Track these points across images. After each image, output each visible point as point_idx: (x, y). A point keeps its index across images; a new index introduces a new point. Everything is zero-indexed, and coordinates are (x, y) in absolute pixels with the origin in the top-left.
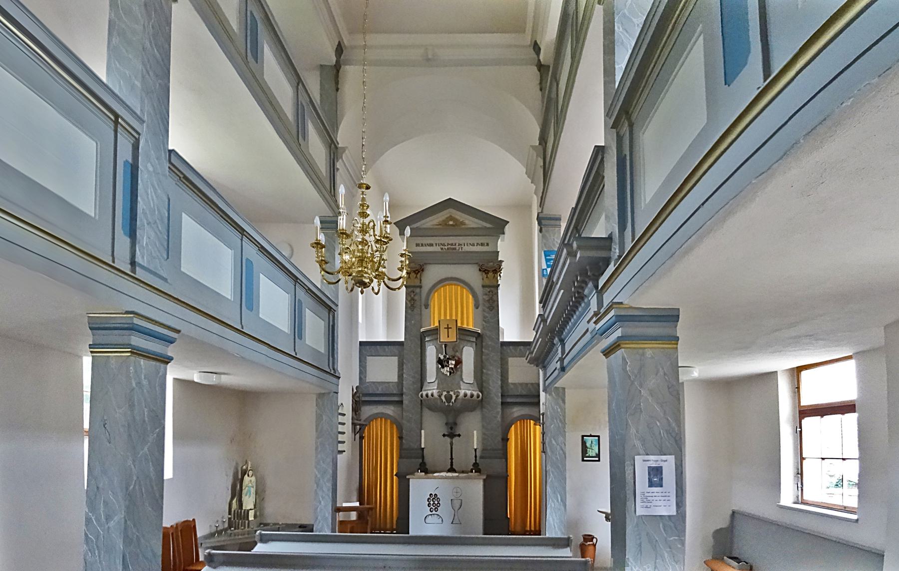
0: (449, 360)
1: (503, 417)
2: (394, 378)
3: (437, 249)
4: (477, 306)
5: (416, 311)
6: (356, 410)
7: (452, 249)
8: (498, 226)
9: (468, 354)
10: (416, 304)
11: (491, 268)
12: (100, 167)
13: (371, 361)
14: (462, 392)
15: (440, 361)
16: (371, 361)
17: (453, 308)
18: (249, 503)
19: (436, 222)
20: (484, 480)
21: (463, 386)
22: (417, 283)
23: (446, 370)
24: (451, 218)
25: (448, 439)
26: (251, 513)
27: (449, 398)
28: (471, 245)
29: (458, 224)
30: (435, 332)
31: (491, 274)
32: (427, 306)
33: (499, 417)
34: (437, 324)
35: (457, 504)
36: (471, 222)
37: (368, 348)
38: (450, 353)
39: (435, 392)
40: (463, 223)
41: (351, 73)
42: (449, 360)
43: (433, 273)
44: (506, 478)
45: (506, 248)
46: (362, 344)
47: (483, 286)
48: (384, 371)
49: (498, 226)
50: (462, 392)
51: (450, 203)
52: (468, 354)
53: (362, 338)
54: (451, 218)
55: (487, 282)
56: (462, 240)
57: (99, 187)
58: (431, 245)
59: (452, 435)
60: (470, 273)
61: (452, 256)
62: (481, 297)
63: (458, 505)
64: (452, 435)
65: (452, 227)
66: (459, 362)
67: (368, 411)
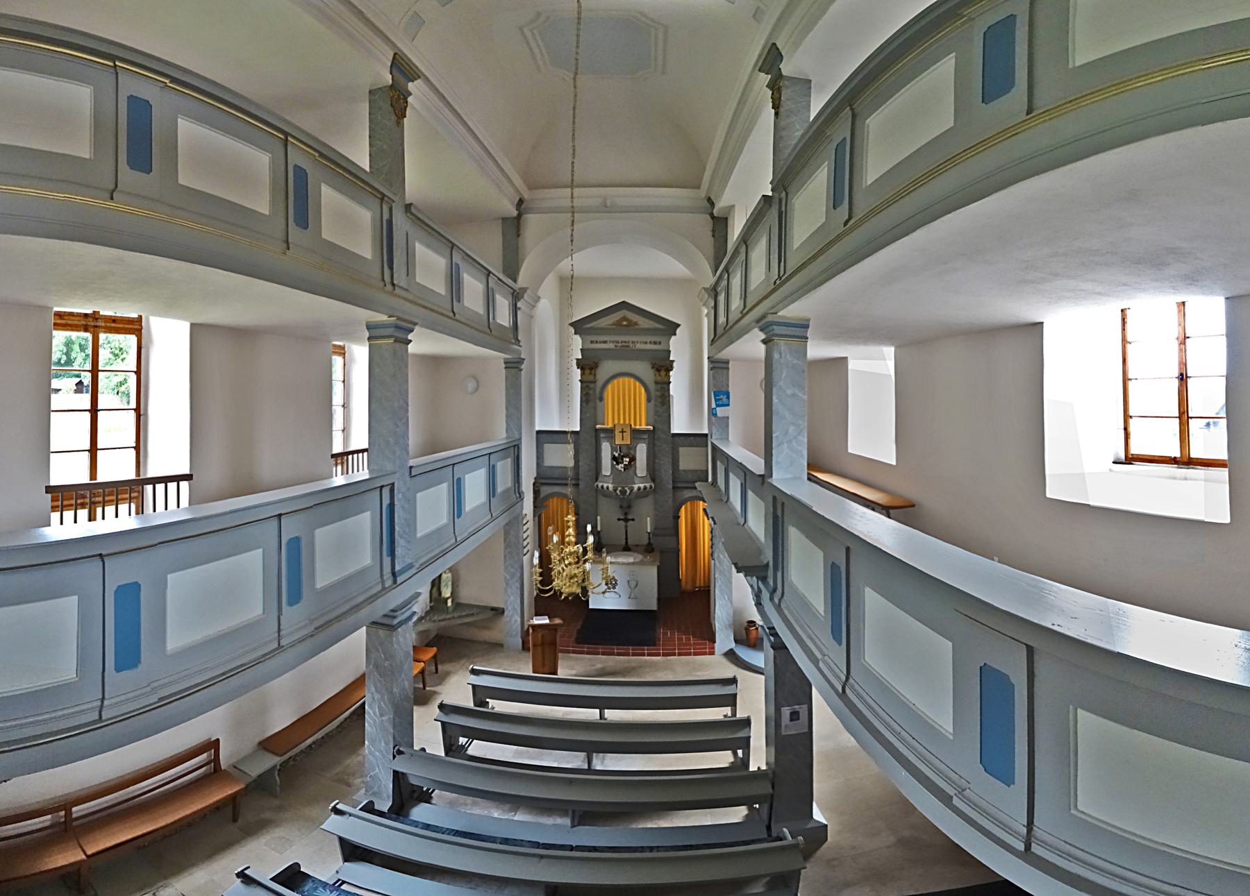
0: (624, 456)
1: (674, 500)
2: (571, 464)
3: (612, 346)
4: (649, 400)
5: (591, 404)
6: (536, 493)
7: (625, 346)
8: (672, 328)
9: (641, 451)
10: (591, 397)
11: (663, 366)
12: (373, 527)
13: (548, 448)
14: (636, 487)
15: (614, 458)
16: (548, 448)
17: (625, 404)
18: (446, 592)
19: (611, 322)
20: (659, 568)
21: (636, 480)
22: (591, 378)
23: (620, 467)
24: (625, 318)
25: (622, 523)
26: (449, 603)
27: (624, 492)
28: (642, 343)
29: (631, 324)
30: (610, 432)
31: (663, 373)
32: (601, 399)
33: (671, 501)
34: (610, 426)
35: (633, 584)
36: (644, 323)
37: (544, 437)
38: (625, 451)
39: (611, 486)
40: (636, 324)
41: (532, 222)
42: (624, 456)
43: (607, 368)
44: (678, 551)
45: (678, 348)
46: (538, 432)
47: (656, 383)
48: (562, 457)
49: (672, 328)
50: (636, 487)
51: (624, 305)
52: (641, 451)
53: (537, 428)
54: (625, 318)
55: (659, 379)
56: (634, 339)
57: (373, 551)
58: (605, 342)
59: (626, 520)
60: (643, 369)
61: (625, 353)
62: (652, 386)
63: (634, 585)
64: (626, 520)
65: (626, 326)
66: (633, 459)
67: (545, 491)
